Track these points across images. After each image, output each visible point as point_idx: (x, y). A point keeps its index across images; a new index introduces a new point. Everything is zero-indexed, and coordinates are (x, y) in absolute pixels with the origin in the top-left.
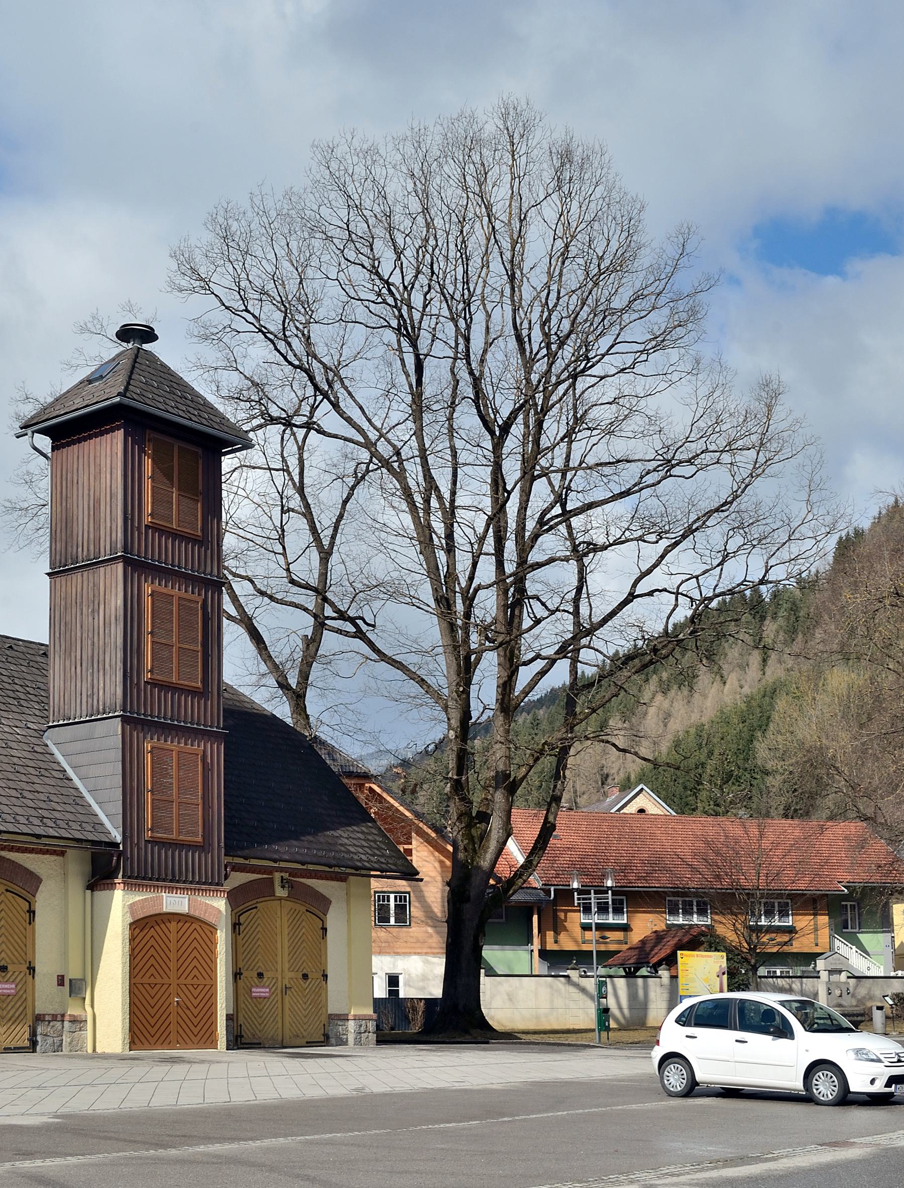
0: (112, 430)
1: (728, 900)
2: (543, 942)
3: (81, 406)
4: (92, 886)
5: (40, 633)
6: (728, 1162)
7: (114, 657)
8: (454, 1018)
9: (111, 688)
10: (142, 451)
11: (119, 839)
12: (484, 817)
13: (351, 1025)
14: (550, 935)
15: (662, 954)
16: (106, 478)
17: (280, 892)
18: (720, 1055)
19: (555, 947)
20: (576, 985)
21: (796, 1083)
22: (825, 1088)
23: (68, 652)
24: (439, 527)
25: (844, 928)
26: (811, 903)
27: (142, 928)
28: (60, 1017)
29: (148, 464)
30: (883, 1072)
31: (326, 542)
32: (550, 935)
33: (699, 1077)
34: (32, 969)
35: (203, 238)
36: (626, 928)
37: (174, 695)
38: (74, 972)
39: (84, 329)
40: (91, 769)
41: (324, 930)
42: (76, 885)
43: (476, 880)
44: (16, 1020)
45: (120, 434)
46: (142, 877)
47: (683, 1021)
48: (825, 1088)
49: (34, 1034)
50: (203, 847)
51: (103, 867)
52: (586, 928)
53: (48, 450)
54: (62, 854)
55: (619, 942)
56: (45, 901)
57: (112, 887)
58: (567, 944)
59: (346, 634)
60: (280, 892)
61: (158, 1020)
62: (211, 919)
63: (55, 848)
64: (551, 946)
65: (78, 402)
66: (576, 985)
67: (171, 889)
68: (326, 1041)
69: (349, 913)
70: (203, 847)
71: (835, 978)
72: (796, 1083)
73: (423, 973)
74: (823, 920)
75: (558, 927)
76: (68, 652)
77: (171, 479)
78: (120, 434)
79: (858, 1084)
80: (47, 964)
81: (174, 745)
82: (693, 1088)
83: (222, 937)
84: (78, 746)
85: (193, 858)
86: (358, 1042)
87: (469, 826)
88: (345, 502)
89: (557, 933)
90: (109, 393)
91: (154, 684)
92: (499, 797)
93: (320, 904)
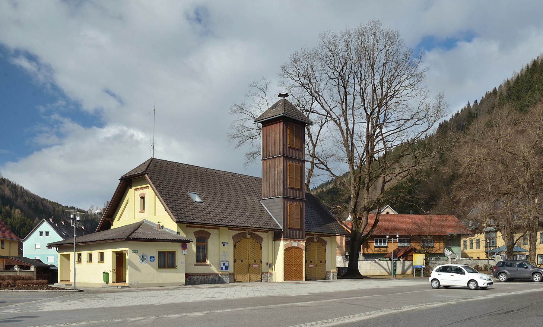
0: (280, 122)
1: (420, 239)
2: (364, 251)
3: (271, 116)
4: (274, 240)
5: (259, 175)
6: (466, 299)
7: (280, 182)
8: (351, 273)
9: (279, 189)
10: (287, 127)
11: (282, 228)
12: (360, 218)
13: (331, 274)
14: (365, 249)
15: (401, 254)
16: (278, 135)
17: (316, 240)
18: (446, 279)
19: (367, 253)
20: (378, 263)
21: (465, 285)
22: (472, 286)
23: (267, 180)
24: (349, 140)
25: (447, 246)
26: (439, 239)
27: (288, 250)
28: (267, 273)
29: (288, 130)
30: (486, 282)
31: (315, 143)
32: (365, 249)
33: (441, 284)
34: (261, 261)
35: (288, 61)
36: (387, 247)
37: (295, 192)
38: (270, 262)
39: (251, 86)
40: (274, 211)
41: (261, 247)
42: (271, 240)
43: (358, 235)
44: (258, 274)
45: (282, 123)
46: (287, 238)
47: (438, 271)
48: (472, 286)
49: (262, 277)
50: (300, 230)
51: (277, 235)
52: (375, 247)
53: (261, 127)
54: (267, 232)
55: (384, 251)
56: (264, 244)
57: (280, 240)
58: (370, 252)
59: (324, 169)
60: (316, 240)
61: (291, 274)
62: (302, 248)
63: (265, 230)
64: (366, 252)
65: (270, 115)
66: (378, 263)
67: (293, 240)
68: (326, 279)
69: (219, 238)
70: (300, 230)
71: (453, 260)
72: (465, 285)
73: (341, 262)
74: (442, 244)
75: (368, 247)
76: (267, 180)
77: (293, 134)
78: (282, 123)
79: (481, 285)
80: (264, 260)
81: (294, 203)
82: (439, 287)
83: (304, 252)
84: (271, 204)
85: (298, 232)
86: (333, 279)
87: (356, 221)
88: (320, 131)
89: (367, 249)
90: (279, 112)
91: (290, 188)
92: (365, 213)
93: (324, 243)
